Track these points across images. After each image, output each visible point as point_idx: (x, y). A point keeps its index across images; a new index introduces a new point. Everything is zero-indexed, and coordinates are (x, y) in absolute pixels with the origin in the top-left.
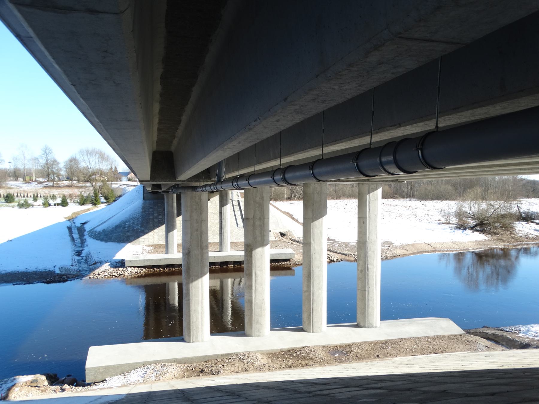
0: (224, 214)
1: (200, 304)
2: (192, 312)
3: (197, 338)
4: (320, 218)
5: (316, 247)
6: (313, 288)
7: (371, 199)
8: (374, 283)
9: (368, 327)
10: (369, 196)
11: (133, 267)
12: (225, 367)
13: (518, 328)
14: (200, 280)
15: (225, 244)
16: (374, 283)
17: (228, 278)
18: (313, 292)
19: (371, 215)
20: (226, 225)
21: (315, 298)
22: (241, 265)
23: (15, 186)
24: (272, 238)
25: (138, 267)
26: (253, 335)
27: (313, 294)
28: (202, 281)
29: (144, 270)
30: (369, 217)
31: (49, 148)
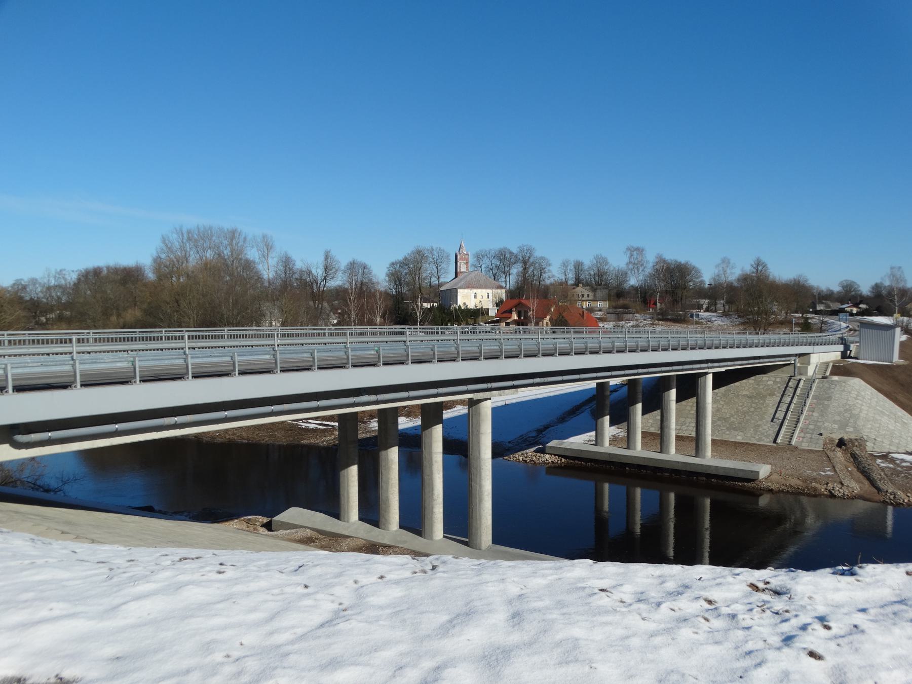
0: (666, 402)
1: (346, 490)
2: (341, 496)
3: (344, 518)
4: (429, 428)
5: (426, 455)
6: (425, 495)
7: (474, 413)
8: (478, 502)
9: (472, 548)
10: (472, 409)
11: (554, 455)
12: (764, 615)
13: (628, 588)
14: (346, 470)
15: (666, 443)
16: (478, 502)
17: (637, 486)
18: (425, 499)
19: (474, 430)
20: (667, 416)
21: (426, 505)
22: (662, 473)
23: (705, 320)
24: (817, 447)
25: (559, 456)
26: (383, 527)
27: (425, 501)
28: (347, 471)
29: (563, 460)
30: (472, 431)
31: (764, 263)
